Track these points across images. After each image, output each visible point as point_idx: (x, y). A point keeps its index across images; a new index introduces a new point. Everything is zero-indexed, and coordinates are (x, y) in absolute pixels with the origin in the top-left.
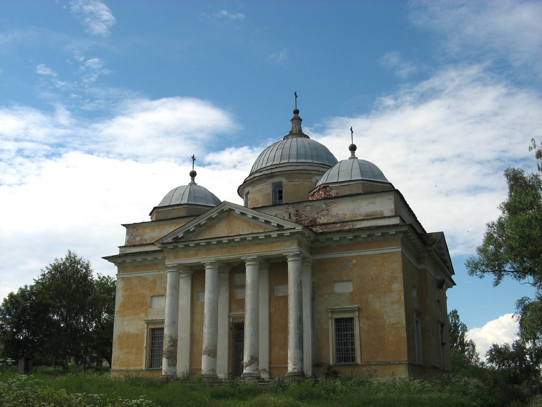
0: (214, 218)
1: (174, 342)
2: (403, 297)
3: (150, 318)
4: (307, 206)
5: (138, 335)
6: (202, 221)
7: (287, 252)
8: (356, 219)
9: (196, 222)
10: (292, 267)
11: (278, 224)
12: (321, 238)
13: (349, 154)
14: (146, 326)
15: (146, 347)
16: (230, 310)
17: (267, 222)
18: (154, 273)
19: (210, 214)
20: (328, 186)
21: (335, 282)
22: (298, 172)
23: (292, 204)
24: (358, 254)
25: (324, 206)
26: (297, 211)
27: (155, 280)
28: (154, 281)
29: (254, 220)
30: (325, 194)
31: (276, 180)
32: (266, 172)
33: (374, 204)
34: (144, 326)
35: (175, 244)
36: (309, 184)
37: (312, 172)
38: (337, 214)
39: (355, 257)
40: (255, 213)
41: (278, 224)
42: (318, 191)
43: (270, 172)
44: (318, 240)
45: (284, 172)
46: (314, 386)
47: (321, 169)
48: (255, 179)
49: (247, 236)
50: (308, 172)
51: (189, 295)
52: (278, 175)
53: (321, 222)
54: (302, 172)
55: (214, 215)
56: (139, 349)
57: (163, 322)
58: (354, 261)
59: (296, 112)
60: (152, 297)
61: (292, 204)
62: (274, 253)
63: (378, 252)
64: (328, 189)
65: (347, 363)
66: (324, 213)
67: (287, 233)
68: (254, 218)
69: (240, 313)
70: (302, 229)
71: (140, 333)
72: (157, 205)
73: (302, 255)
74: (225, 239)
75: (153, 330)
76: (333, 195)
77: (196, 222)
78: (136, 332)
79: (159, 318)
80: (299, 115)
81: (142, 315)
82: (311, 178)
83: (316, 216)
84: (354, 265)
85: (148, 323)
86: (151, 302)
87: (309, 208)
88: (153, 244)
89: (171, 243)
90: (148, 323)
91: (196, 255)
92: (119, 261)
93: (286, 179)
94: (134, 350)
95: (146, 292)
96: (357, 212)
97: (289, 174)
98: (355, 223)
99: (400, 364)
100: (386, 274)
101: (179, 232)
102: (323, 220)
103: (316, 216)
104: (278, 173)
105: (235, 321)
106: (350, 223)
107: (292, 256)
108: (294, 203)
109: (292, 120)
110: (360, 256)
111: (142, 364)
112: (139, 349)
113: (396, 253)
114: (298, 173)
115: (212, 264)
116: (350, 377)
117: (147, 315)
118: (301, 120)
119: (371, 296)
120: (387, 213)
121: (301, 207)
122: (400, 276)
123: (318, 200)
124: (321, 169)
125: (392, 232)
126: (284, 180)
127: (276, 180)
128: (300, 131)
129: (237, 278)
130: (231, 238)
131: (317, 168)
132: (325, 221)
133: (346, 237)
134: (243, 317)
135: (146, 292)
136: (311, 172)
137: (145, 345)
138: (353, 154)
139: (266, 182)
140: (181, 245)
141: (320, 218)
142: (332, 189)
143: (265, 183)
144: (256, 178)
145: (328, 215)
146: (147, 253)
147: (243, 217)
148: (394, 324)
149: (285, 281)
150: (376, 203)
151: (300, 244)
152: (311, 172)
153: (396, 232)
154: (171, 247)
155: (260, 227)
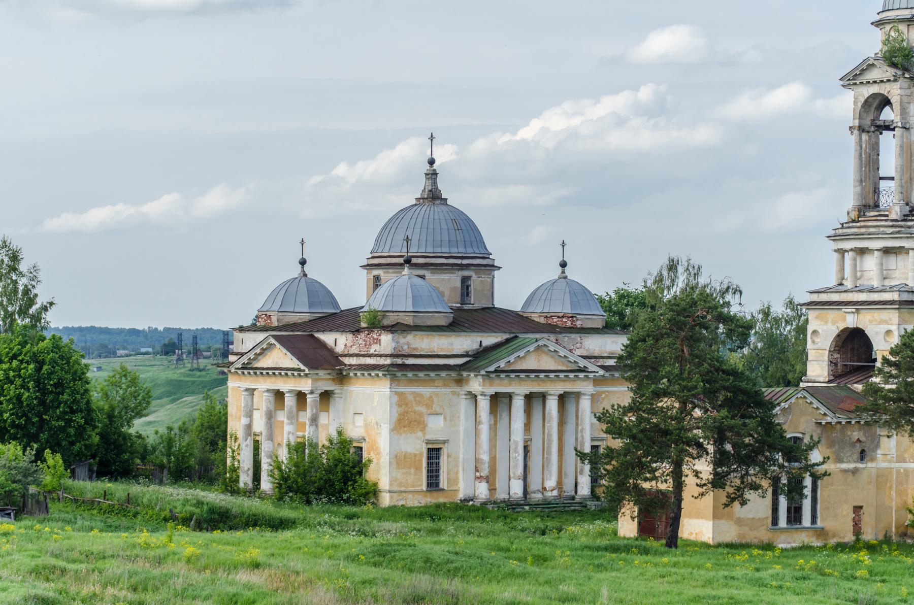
3: (429, 437)
5: (415, 455)
14: (424, 445)
18: (431, 390)
25: (579, 339)
27: (431, 397)
28: (431, 398)
30: (572, 324)
34: (422, 445)
39: (603, 392)
56: (418, 468)
58: (603, 396)
64: (574, 319)
65: (433, 489)
66: (578, 345)
71: (417, 453)
75: (428, 449)
78: (414, 451)
80: (435, 166)
81: (420, 434)
83: (572, 347)
84: (603, 399)
91: (510, 385)
93: (476, 273)
94: (413, 470)
95: (423, 409)
96: (603, 349)
103: (572, 347)
110: (608, 391)
111: (421, 485)
112: (418, 468)
116: (729, 500)
117: (424, 434)
127: (466, 273)
135: (423, 409)
138: (563, 272)
139: (455, 273)
142: (577, 320)
143: (453, 273)
146: (357, 355)
155: (563, 364)
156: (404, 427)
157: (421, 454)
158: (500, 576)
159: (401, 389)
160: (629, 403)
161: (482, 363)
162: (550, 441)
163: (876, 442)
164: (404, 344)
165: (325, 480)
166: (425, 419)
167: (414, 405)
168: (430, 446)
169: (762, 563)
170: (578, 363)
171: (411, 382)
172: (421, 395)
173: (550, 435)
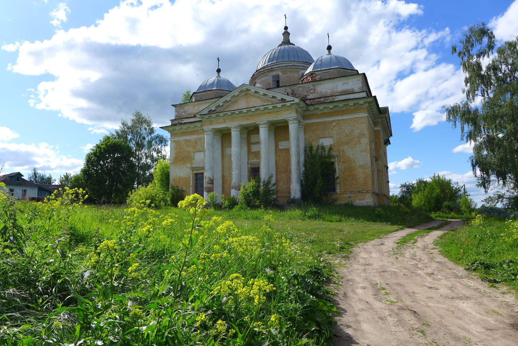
0: (236, 96)
1: (212, 182)
2: (369, 147)
3: (194, 166)
4: (300, 87)
5: (186, 178)
6: (228, 98)
7: (286, 118)
8: (335, 95)
9: (224, 99)
10: (293, 127)
11: (281, 98)
12: (311, 108)
13: (327, 51)
15: (192, 186)
16: (249, 159)
17: (273, 97)
19: (233, 93)
20: (314, 73)
21: (320, 138)
22: (290, 67)
23: (289, 86)
24: (337, 119)
25: (312, 87)
26: (293, 91)
27: (196, 141)
28: (196, 142)
29: (264, 97)
30: (312, 79)
31: (275, 73)
32: (268, 68)
33: (347, 84)
35: (210, 115)
36: (297, 75)
37: (300, 67)
38: (321, 92)
39: (333, 121)
40: (266, 92)
41: (281, 98)
42: (307, 78)
43: (270, 68)
44: (309, 110)
45: (280, 68)
46: (486, 192)
47: (305, 65)
48: (260, 73)
49: (260, 108)
50: (297, 67)
51: (220, 150)
52: (275, 70)
53: (310, 98)
54: (292, 67)
55: (236, 93)
57: (203, 168)
58: (334, 124)
59: (286, 28)
60: (194, 152)
61: (289, 86)
62: (280, 118)
63: (351, 117)
64: (314, 75)
66: (312, 91)
67: (288, 104)
68: (264, 95)
69: (256, 161)
70: (299, 101)
72: (195, 91)
73: (299, 119)
74: (245, 110)
75: (196, 174)
76: (318, 79)
77: (224, 99)
79: (201, 165)
80: (288, 30)
81: (189, 165)
82: (298, 72)
84: (334, 126)
85: (193, 169)
86: (194, 155)
87: (301, 88)
88: (195, 116)
89: (207, 114)
90: (193, 169)
91: (225, 122)
92: (171, 129)
95: (190, 149)
96: (335, 90)
97: (283, 69)
98: (334, 97)
99: (367, 192)
100: (357, 131)
101: (212, 107)
102: (311, 96)
103: (306, 94)
104: (276, 69)
105: (252, 166)
106: (330, 98)
107: (292, 120)
108: (291, 85)
109: (283, 34)
110: (338, 120)
113: (364, 117)
114: (290, 68)
115: (236, 127)
117: (191, 164)
118: (289, 34)
119: (346, 147)
120: (356, 90)
121: (295, 88)
122: (367, 133)
123: (306, 83)
124: (305, 65)
125: (361, 102)
126: (280, 74)
128: (289, 41)
129: (253, 138)
130: (249, 109)
131: (303, 65)
132: (313, 97)
133: (328, 107)
134: (259, 164)
135: (190, 149)
136: (298, 67)
137: (191, 184)
138: (329, 52)
140: (214, 115)
141: (309, 95)
142: (316, 75)
144: (262, 73)
145: (314, 92)
147: (256, 95)
148: (363, 166)
149: (287, 138)
150: (348, 83)
151: (297, 112)
152: (298, 67)
153: (364, 102)
154: (207, 117)
155: (269, 101)
156: (179, 161)
157: (190, 177)
158: (190, 270)
159: (176, 139)
160: (133, 120)
161: (345, 117)
162: (230, 169)
163: (108, 163)
164: (183, 112)
165: (77, 203)
166: (192, 155)
167: (185, 147)
168: (196, 172)
169: (478, 255)
170: (276, 97)
171: (184, 134)
172: (189, 141)
173: (230, 162)
